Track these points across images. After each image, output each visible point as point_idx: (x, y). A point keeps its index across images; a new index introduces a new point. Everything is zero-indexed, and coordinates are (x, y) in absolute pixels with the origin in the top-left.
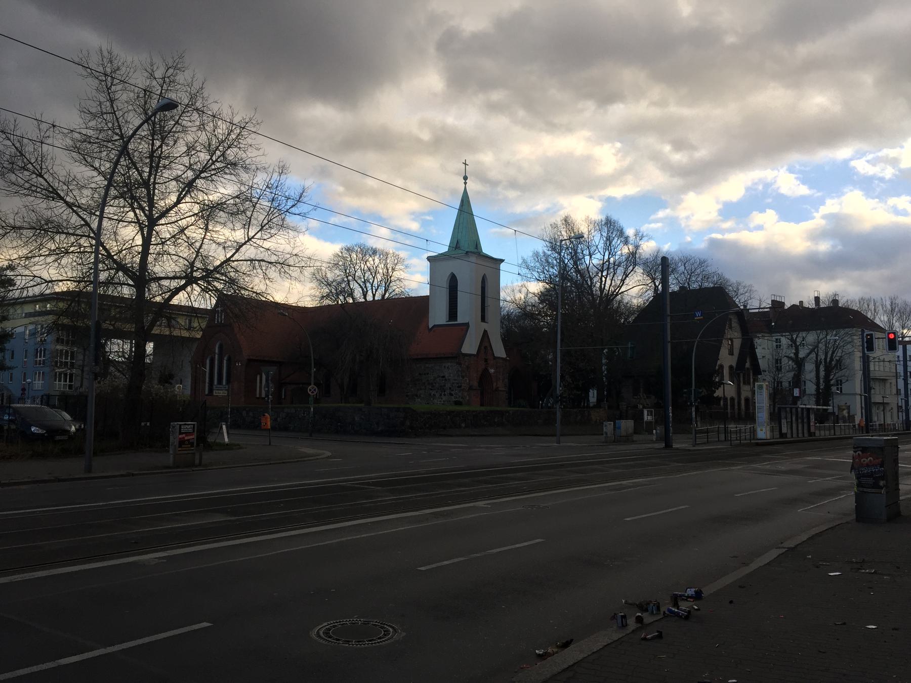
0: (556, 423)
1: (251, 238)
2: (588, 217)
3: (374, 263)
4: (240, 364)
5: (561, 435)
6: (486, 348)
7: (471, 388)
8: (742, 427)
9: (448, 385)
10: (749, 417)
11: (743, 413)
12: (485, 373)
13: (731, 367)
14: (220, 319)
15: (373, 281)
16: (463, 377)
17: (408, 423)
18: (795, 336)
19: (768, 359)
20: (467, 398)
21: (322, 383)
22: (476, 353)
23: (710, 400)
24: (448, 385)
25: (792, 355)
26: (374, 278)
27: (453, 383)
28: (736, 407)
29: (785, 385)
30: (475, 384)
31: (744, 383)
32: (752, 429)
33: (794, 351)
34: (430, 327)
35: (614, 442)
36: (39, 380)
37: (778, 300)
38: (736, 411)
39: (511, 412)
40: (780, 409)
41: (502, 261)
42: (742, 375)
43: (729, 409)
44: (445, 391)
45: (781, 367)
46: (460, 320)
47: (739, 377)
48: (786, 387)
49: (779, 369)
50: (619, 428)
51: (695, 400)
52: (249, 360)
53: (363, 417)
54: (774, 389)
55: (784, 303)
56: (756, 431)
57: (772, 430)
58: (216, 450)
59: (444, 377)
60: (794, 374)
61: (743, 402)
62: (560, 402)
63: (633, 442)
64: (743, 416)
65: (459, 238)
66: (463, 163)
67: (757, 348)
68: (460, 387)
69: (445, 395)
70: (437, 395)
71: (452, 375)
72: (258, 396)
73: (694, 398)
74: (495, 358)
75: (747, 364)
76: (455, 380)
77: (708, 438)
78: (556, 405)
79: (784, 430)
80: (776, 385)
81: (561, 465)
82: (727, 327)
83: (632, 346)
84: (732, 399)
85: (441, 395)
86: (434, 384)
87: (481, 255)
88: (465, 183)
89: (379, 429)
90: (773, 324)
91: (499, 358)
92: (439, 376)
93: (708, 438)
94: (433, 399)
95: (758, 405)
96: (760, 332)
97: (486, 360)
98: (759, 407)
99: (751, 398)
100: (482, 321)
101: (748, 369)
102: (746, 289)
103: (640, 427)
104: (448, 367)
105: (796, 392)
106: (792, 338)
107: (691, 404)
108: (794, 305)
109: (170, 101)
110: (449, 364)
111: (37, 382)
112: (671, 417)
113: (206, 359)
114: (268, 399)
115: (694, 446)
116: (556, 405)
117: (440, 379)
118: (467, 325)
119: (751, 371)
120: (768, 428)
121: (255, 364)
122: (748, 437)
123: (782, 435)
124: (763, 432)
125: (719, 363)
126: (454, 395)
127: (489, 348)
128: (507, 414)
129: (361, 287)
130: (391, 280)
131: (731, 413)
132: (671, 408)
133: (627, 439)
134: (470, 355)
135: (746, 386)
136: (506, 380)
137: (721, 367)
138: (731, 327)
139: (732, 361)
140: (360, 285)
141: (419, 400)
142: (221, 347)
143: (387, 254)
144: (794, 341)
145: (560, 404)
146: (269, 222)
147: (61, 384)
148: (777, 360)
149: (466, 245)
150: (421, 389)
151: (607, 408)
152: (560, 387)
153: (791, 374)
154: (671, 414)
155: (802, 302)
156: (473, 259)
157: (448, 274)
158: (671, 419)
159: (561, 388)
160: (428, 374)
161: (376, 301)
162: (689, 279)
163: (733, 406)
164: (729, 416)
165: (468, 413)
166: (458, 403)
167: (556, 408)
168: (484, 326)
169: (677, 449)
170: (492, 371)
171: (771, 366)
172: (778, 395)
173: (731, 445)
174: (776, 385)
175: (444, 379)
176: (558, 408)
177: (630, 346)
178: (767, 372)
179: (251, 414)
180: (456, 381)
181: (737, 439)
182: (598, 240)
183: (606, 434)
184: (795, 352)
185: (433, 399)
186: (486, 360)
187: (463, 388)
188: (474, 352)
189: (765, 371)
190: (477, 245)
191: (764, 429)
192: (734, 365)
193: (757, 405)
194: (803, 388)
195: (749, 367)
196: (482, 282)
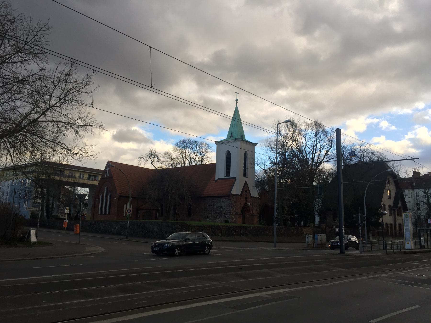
0: (274, 235)
1: (52, 107)
2: (305, 121)
4: (115, 198)
5: (277, 242)
6: (246, 191)
7: (236, 214)
8: (395, 241)
9: (224, 212)
10: (401, 235)
11: (398, 233)
12: (246, 204)
13: (390, 206)
14: (107, 175)
16: (232, 207)
18: (427, 191)
19: (412, 203)
24: (224, 212)
25: (426, 201)
26: (196, 156)
27: (227, 211)
28: (394, 229)
29: (422, 217)
30: (239, 211)
31: (398, 215)
32: (401, 243)
33: (426, 199)
34: (216, 179)
35: (313, 247)
36: (25, 206)
37: (417, 171)
38: (394, 231)
39: (252, 228)
40: (419, 230)
42: (396, 210)
44: (222, 215)
45: (419, 207)
46: (232, 176)
47: (395, 212)
49: (418, 209)
50: (317, 239)
51: (361, 223)
52: (120, 196)
53: (158, 228)
54: (416, 219)
55: (420, 173)
56: (404, 243)
57: (415, 244)
58: (20, 247)
59: (221, 207)
61: (397, 226)
66: (236, 92)
67: (405, 197)
68: (230, 212)
70: (218, 217)
71: (226, 206)
74: (251, 197)
76: (227, 209)
78: (274, 223)
79: (423, 244)
80: (417, 217)
82: (387, 183)
83: (321, 187)
85: (220, 217)
87: (243, 140)
88: (237, 103)
89: (167, 235)
90: (414, 184)
91: (254, 197)
92: (219, 207)
94: (216, 219)
96: (407, 188)
97: (246, 198)
98: (406, 229)
99: (402, 224)
100: (244, 177)
102: (398, 164)
104: (224, 201)
106: (425, 191)
107: (359, 225)
108: (425, 174)
110: (225, 200)
111: (24, 207)
113: (100, 195)
114: (80, 214)
116: (274, 223)
118: (235, 178)
120: (412, 242)
121: (124, 198)
122: (399, 248)
123: (422, 247)
124: (409, 245)
125: (382, 203)
127: (248, 192)
128: (249, 228)
129: (189, 161)
130: (204, 158)
132: (343, 227)
133: (322, 246)
134: (236, 195)
135: (399, 217)
136: (258, 210)
138: (389, 183)
139: (391, 202)
141: (208, 219)
142: (107, 189)
143: (203, 144)
145: (276, 223)
146: (65, 96)
147: (420, 218)
148: (417, 204)
149: (235, 135)
150: (209, 214)
152: (277, 212)
155: (430, 172)
156: (239, 143)
157: (226, 151)
159: (277, 213)
160: (213, 205)
162: (363, 155)
163: (391, 228)
166: (226, 222)
168: (245, 179)
169: (348, 255)
170: (249, 204)
171: (414, 206)
174: (417, 217)
175: (222, 208)
176: (275, 226)
177: (318, 187)
178: (412, 210)
179: (104, 225)
181: (392, 249)
182: (311, 133)
183: (308, 242)
185: (216, 219)
186: (246, 198)
187: (232, 213)
189: (411, 210)
190: (242, 135)
191: (410, 243)
192: (392, 205)
193: (404, 227)
195: (401, 206)
196: (244, 155)
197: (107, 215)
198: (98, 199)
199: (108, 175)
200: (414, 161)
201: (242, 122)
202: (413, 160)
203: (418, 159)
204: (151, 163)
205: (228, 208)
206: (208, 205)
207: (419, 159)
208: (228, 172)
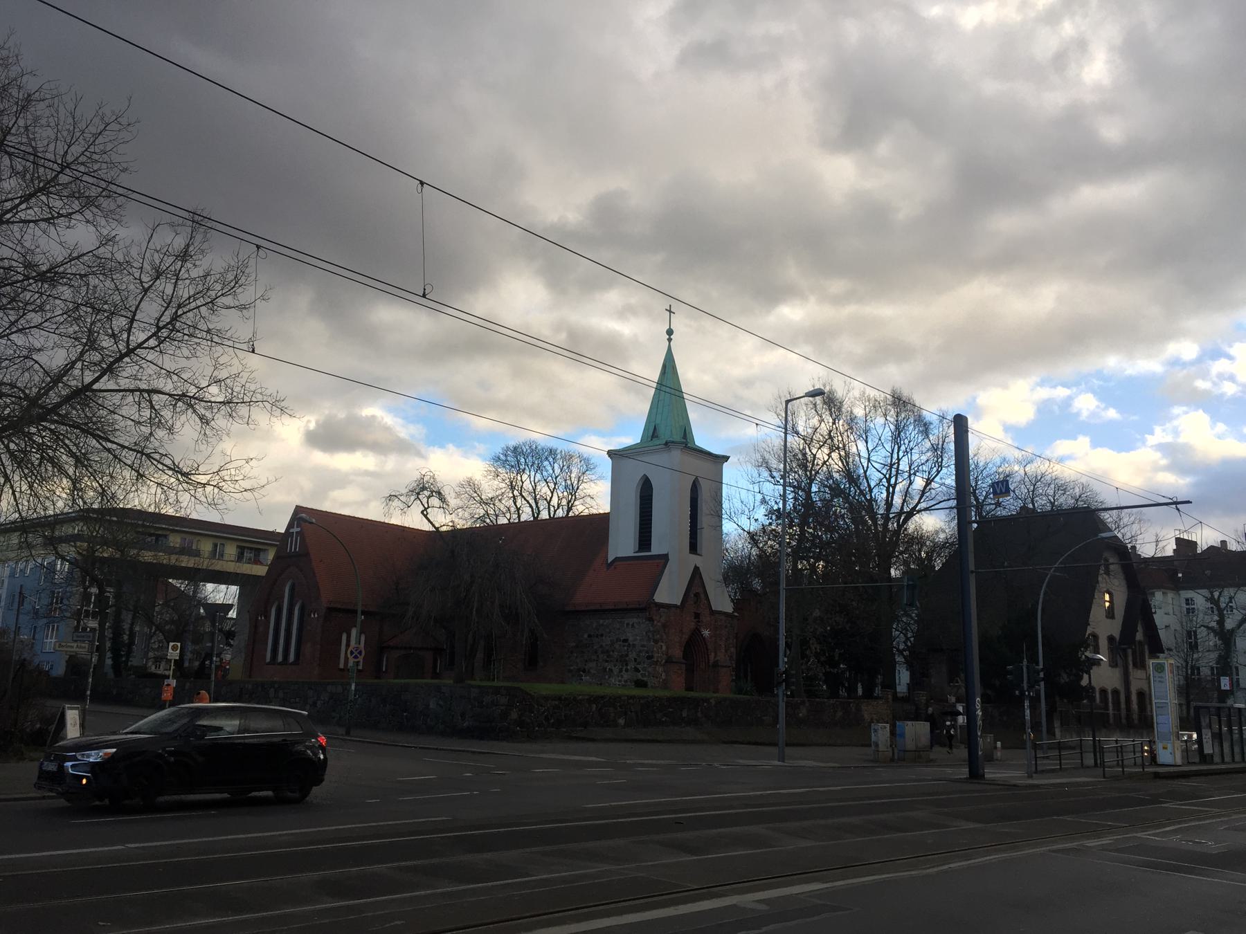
3: (554, 472)
4: (316, 616)
6: (697, 595)
7: (669, 661)
9: (632, 655)
10: (1143, 723)
11: (1135, 716)
13: (1111, 639)
14: (293, 546)
15: (551, 498)
16: (656, 642)
17: (514, 715)
20: (663, 677)
21: (445, 647)
22: (679, 604)
23: (1077, 693)
25: (1214, 624)
28: (1123, 706)
29: (1205, 671)
30: (677, 653)
31: (1135, 665)
33: (1216, 618)
35: (892, 760)
36: (51, 638)
38: (1123, 712)
39: (713, 701)
41: (726, 458)
42: (1130, 652)
43: (1111, 708)
44: (627, 665)
45: (1196, 643)
46: (656, 549)
47: (1126, 656)
48: (1206, 676)
49: (1194, 647)
50: (902, 735)
53: (441, 703)
54: (1186, 678)
59: (625, 641)
60: (1220, 656)
61: (1134, 697)
62: (784, 683)
63: (929, 762)
64: (1136, 722)
65: (658, 422)
69: (627, 670)
70: (616, 670)
71: (638, 638)
72: (341, 666)
73: (1028, 682)
74: (713, 613)
75: (1137, 634)
77: (1060, 760)
81: (678, 822)
82: (1101, 572)
83: (911, 583)
84: (1116, 692)
85: (621, 671)
86: (611, 653)
87: (689, 447)
88: (670, 340)
90: (1180, 575)
93: (1060, 764)
94: (609, 677)
95: (1156, 701)
97: (697, 616)
98: (1158, 705)
101: (1140, 642)
103: (941, 738)
105: (1225, 683)
107: (1022, 693)
108: (1212, 547)
109: (1148, 692)
110: (635, 620)
111: (49, 640)
112: (979, 718)
115: (1030, 777)
116: (777, 689)
117: (620, 645)
118: (665, 558)
119: (1146, 647)
121: (340, 616)
126: (642, 672)
127: (702, 596)
129: (531, 506)
130: (575, 498)
131: (1114, 714)
133: (918, 757)
134: (668, 606)
135: (1139, 671)
137: (1095, 637)
138: (1107, 572)
139: (1113, 628)
140: (528, 502)
141: (588, 678)
143: (571, 457)
144: (1215, 602)
148: (1189, 634)
151: (890, 700)
153: (1214, 656)
154: (979, 713)
156: (676, 455)
158: (980, 722)
159: (786, 660)
160: (602, 635)
161: (522, 522)
162: (1033, 491)
163: (1117, 703)
164: (1111, 721)
165: (631, 701)
166: (640, 684)
167: (777, 695)
168: (695, 560)
169: (993, 783)
170: (706, 633)
172: (1190, 687)
173: (1104, 777)
175: (626, 644)
180: (645, 648)
183: (877, 745)
184: (1218, 619)
185: (609, 677)
186: (697, 616)
188: (677, 601)
190: (686, 433)
191: (1169, 746)
192: (1117, 634)
194: (1235, 677)
197: (291, 664)
198: (265, 617)
199: (295, 548)
200: (1178, 509)
201: (685, 396)
202: (1174, 506)
203: (1189, 502)
204: (422, 512)
205: (645, 643)
206: (586, 636)
207: (1191, 502)
208: (645, 539)
